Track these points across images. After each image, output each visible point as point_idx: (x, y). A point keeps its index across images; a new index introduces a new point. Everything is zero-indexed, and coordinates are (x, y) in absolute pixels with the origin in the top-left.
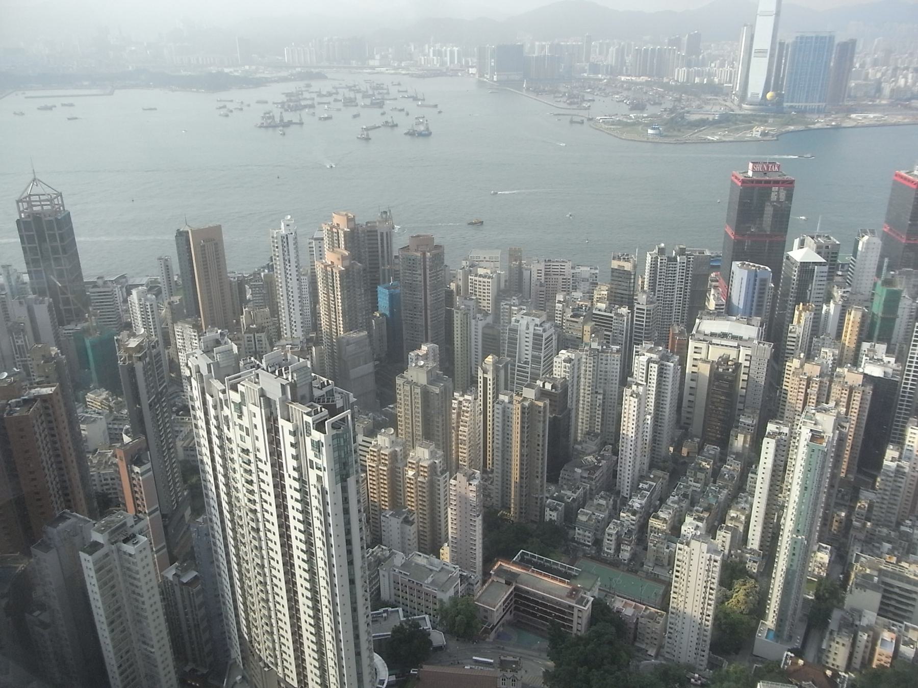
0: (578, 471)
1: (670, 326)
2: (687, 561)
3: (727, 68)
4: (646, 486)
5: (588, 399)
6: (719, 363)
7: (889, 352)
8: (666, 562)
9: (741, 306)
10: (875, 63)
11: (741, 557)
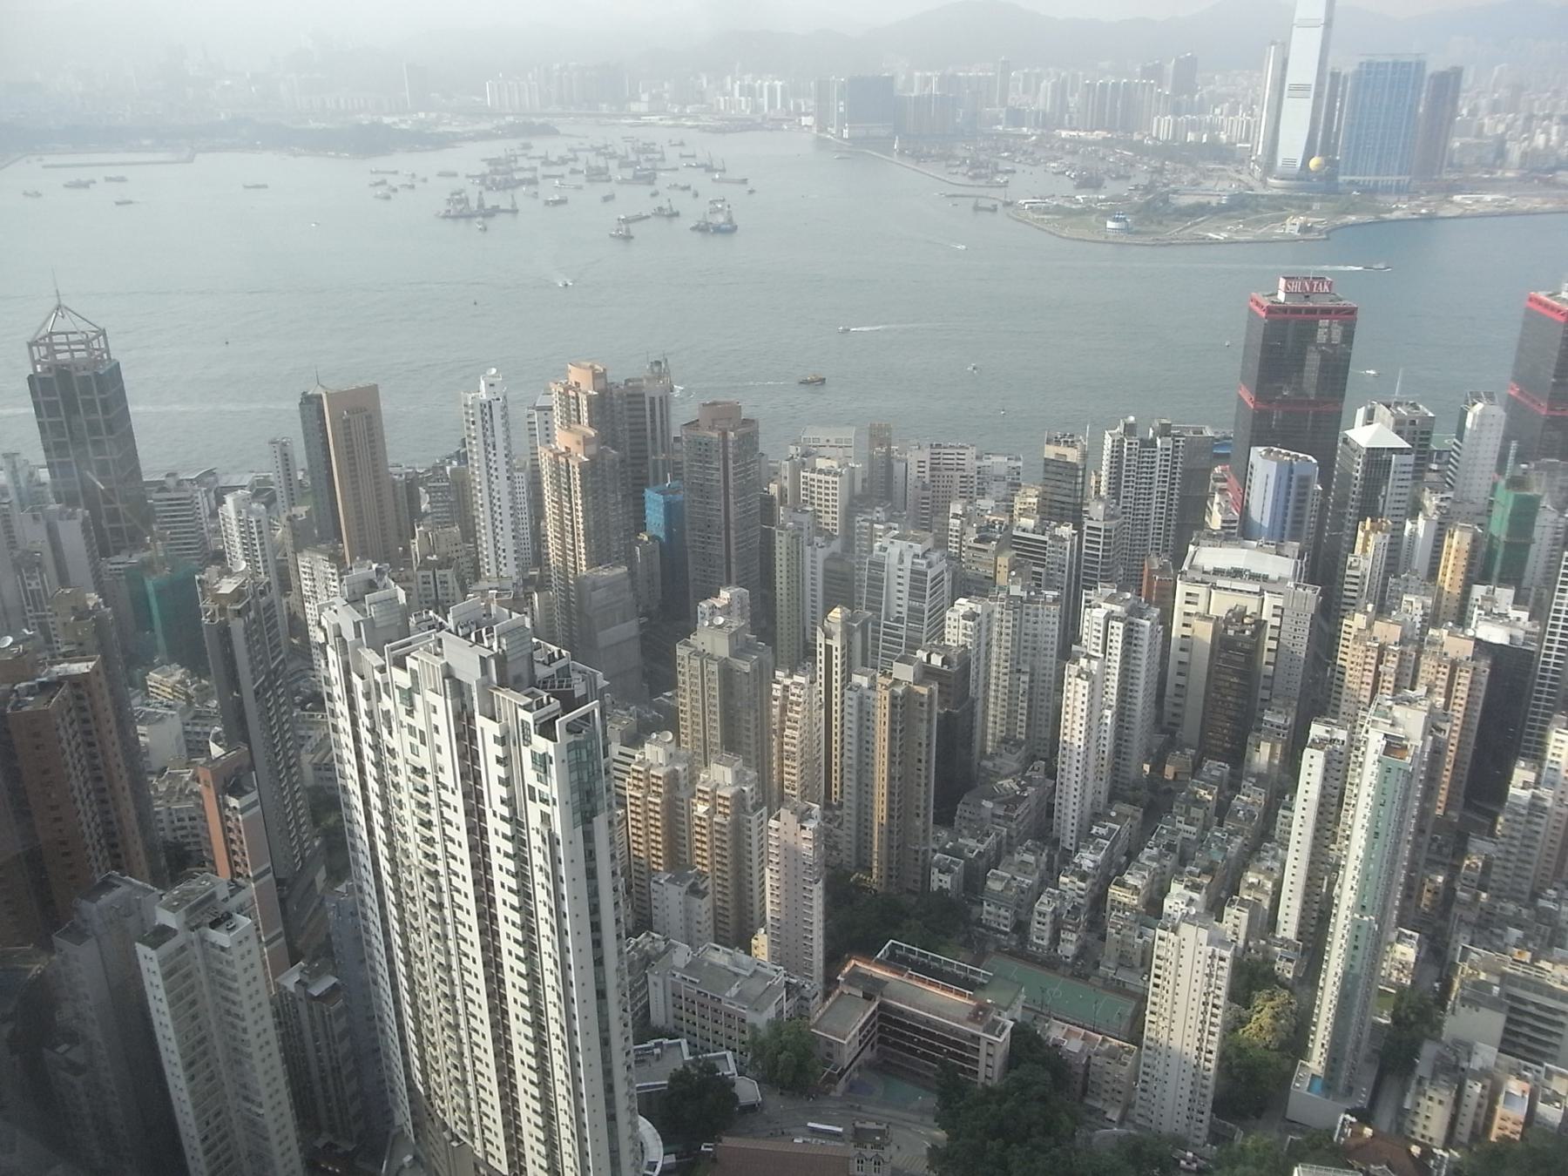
0: (988, 804)
1: (1144, 558)
2: (1173, 959)
3: (1242, 116)
4: (1103, 831)
5: (1005, 681)
6: (1227, 621)
7: (1518, 601)
8: (1137, 961)
9: (1266, 524)
10: (1494, 108)
11: (1266, 951)
